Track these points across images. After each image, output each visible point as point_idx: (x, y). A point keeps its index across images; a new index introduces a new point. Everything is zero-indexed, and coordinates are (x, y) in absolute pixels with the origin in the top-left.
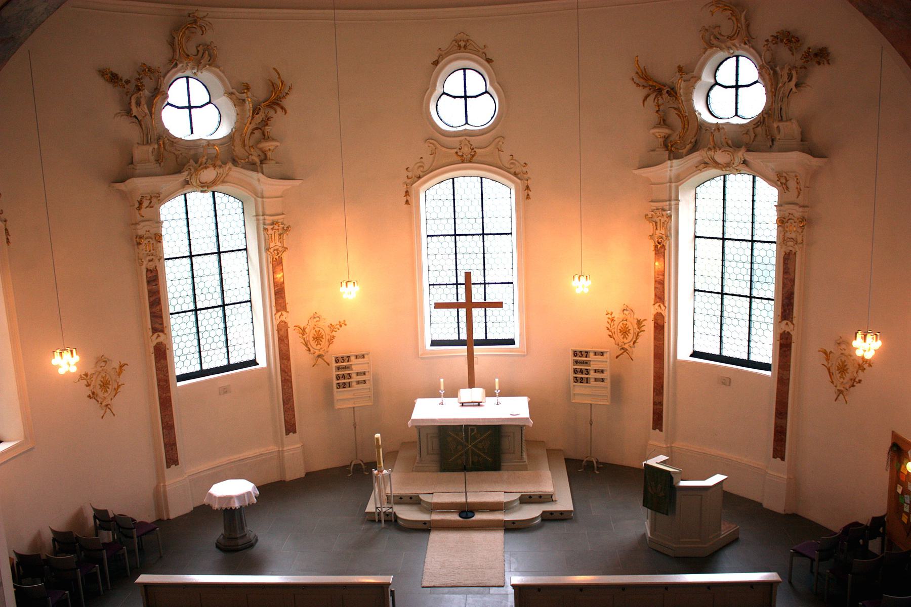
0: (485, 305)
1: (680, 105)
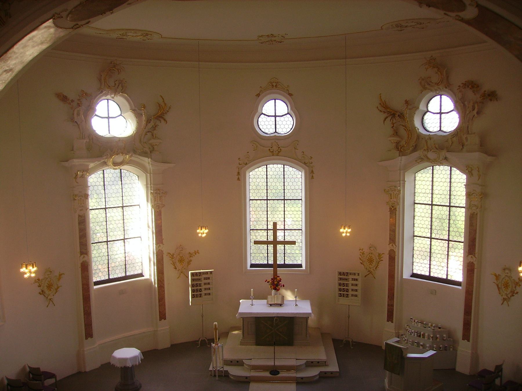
0: (284, 243)
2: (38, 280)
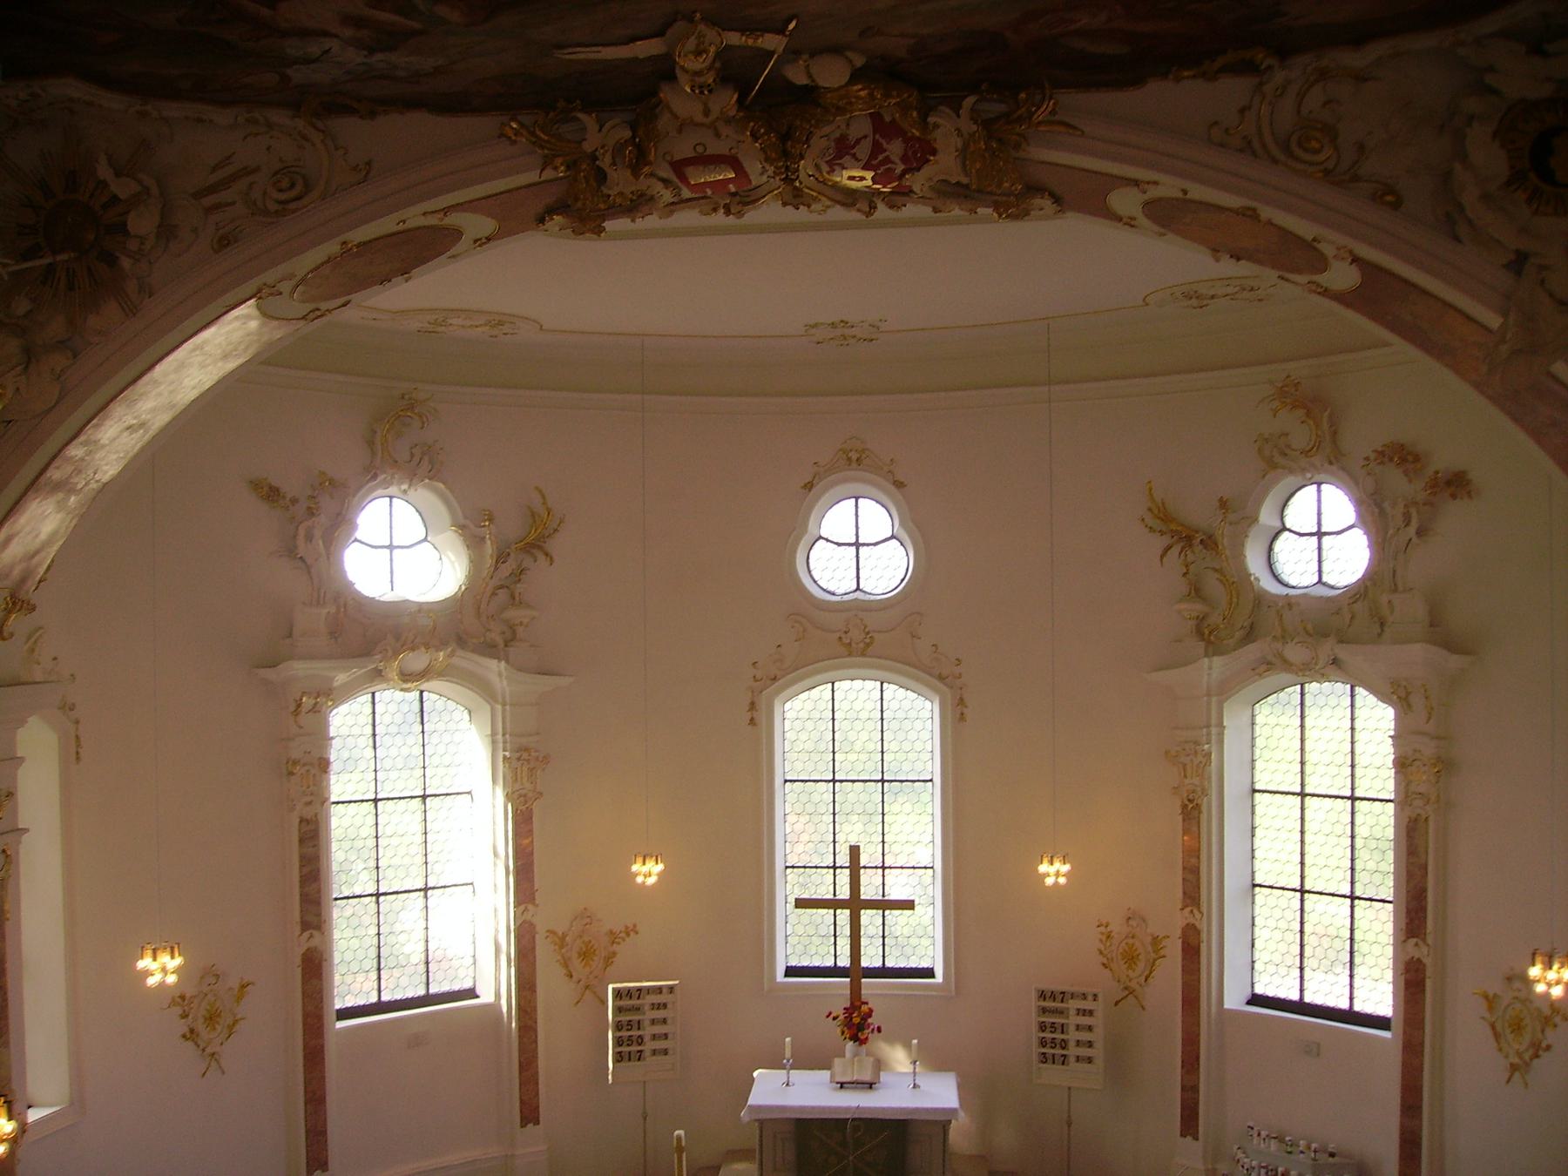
0: (884, 905)
1: (1225, 564)
2: (180, 997)
